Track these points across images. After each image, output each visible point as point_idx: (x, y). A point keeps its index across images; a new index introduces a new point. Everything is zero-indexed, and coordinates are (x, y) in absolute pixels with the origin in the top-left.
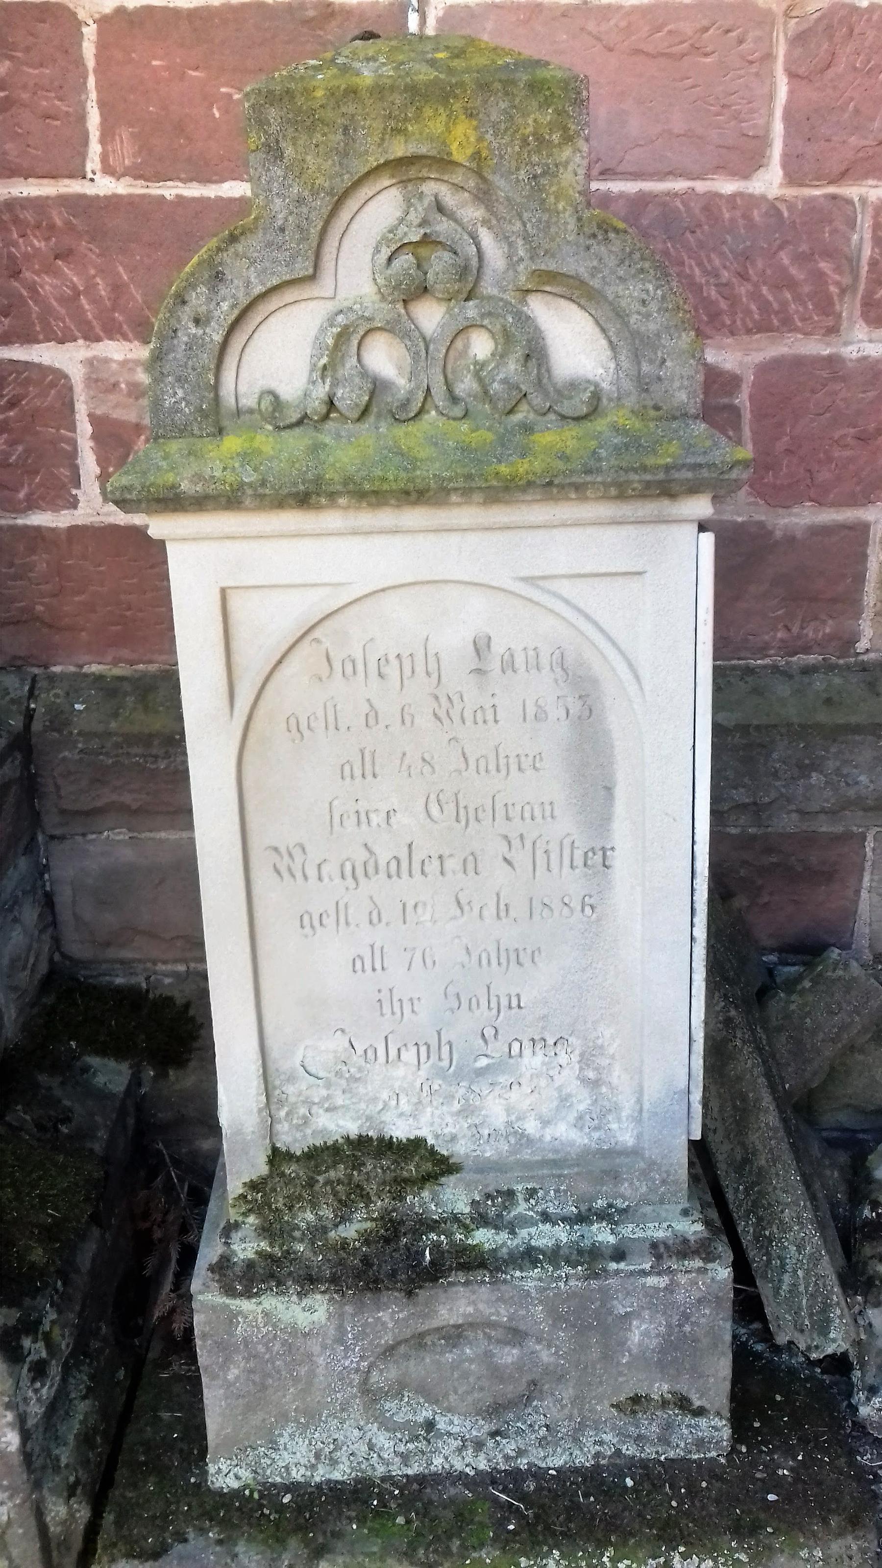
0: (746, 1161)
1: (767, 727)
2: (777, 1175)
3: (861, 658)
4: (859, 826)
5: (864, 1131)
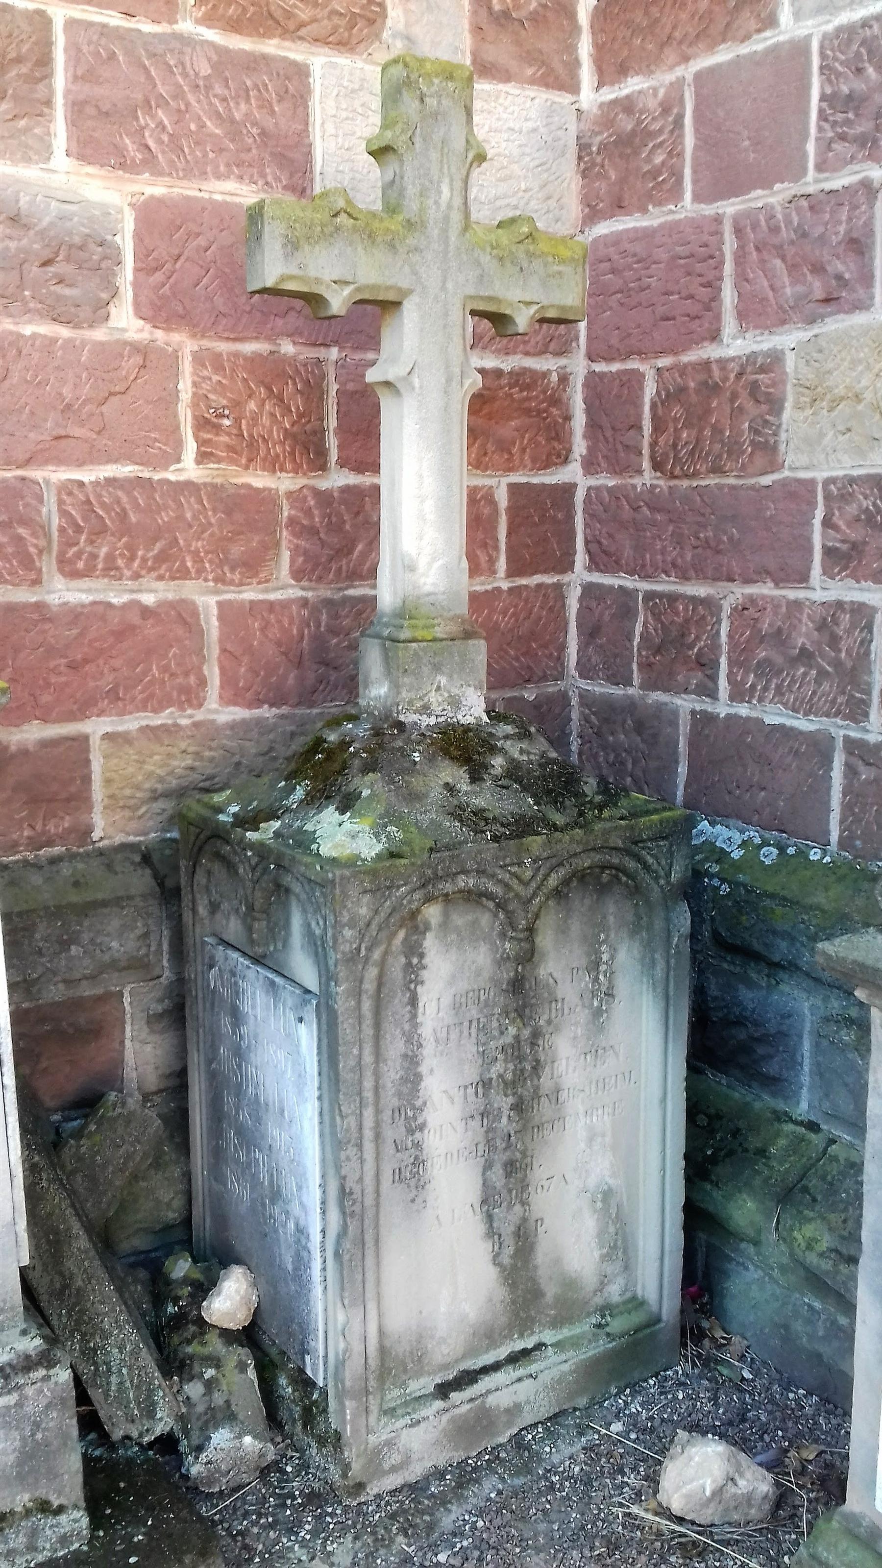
0: (65, 1287)
1: (27, 912)
2: (94, 1290)
3: (97, 845)
4: (116, 986)
5: (156, 1250)
